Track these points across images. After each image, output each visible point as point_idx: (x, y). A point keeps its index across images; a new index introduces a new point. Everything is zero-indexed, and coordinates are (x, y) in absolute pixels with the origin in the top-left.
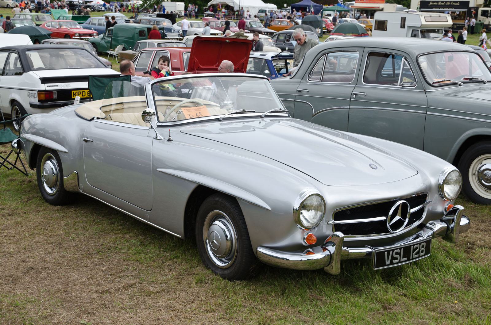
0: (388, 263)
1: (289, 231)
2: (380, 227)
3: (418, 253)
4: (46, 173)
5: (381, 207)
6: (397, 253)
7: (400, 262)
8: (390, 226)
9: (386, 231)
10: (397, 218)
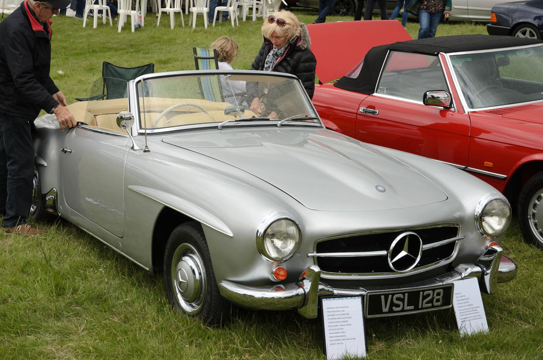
0: (385, 310)
1: (250, 263)
2: (379, 265)
3: (431, 301)
4: (182, 279)
5: (380, 238)
6: (398, 299)
7: (403, 310)
8: (392, 264)
9: (388, 270)
10: (403, 254)
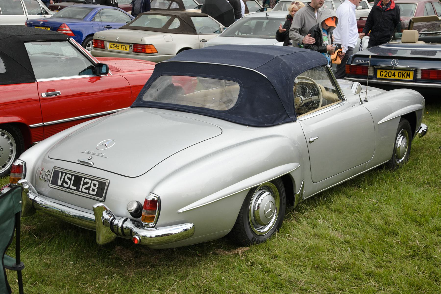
3: (88, 188)
6: (68, 178)
